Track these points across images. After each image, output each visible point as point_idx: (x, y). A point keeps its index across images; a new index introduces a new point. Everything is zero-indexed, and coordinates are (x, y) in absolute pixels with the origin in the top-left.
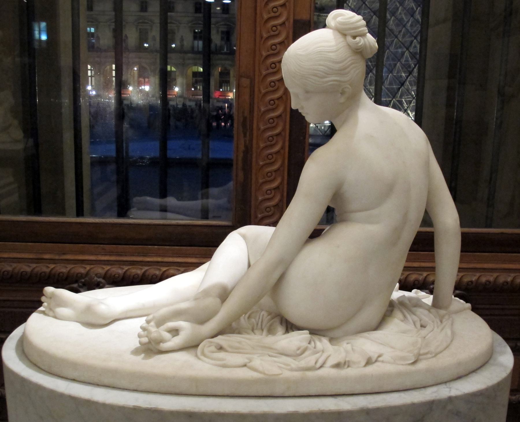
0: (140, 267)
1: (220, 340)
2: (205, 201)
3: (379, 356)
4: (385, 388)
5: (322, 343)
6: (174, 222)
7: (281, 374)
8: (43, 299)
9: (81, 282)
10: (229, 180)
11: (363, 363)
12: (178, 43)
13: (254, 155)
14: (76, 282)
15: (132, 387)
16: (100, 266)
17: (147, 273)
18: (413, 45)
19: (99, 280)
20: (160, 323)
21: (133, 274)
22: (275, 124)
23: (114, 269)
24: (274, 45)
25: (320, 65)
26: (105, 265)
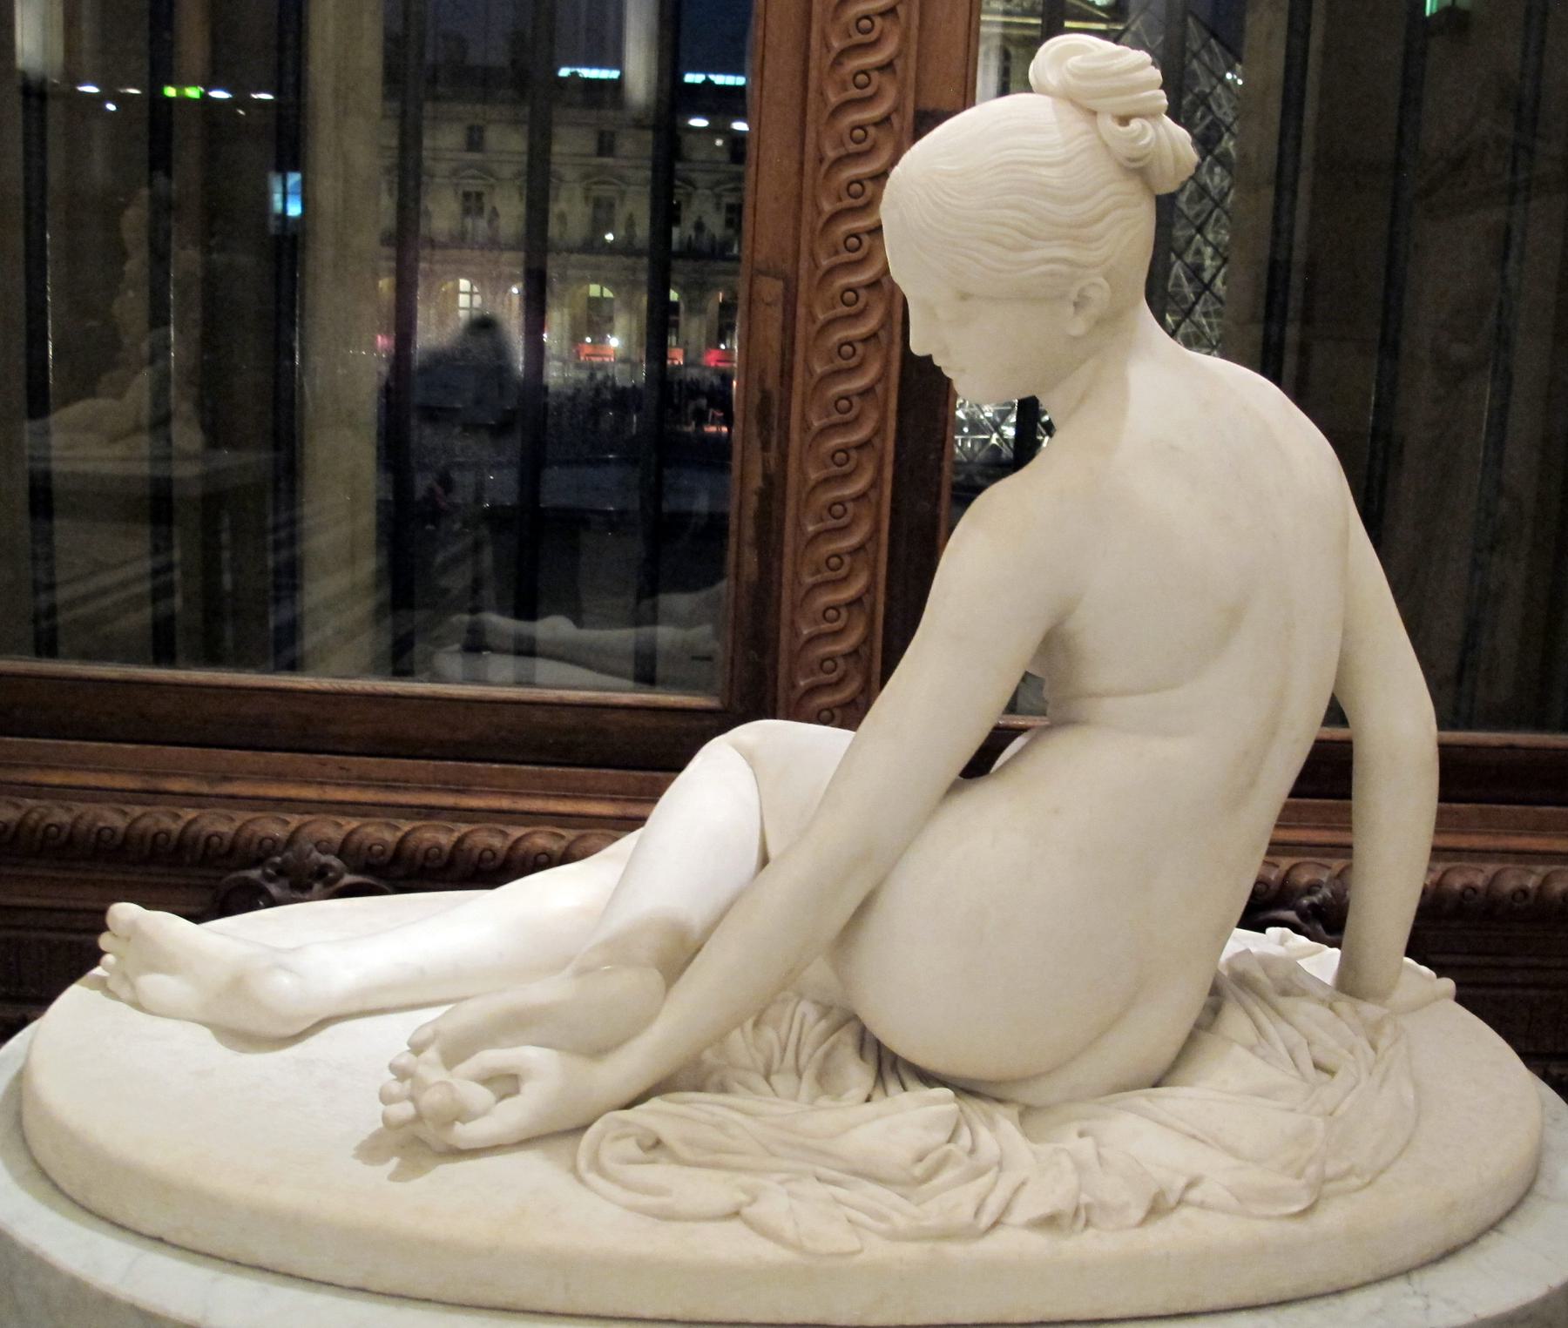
1: (656, 1115)
2: (646, 630)
3: (1190, 1185)
4: (1209, 1302)
5: (997, 1132)
6: (551, 695)
7: (860, 1251)
8: (104, 941)
9: (273, 865)
10: (720, 576)
11: (1137, 1214)
12: (622, 233)
13: (791, 504)
14: (258, 862)
15: (351, 1276)
16: (332, 818)
17: (467, 844)
18: (1193, 247)
19: (324, 859)
20: (455, 1053)
21: (425, 845)
22: (852, 463)
24: (867, 17)
25: (1009, 207)
26: (345, 814)
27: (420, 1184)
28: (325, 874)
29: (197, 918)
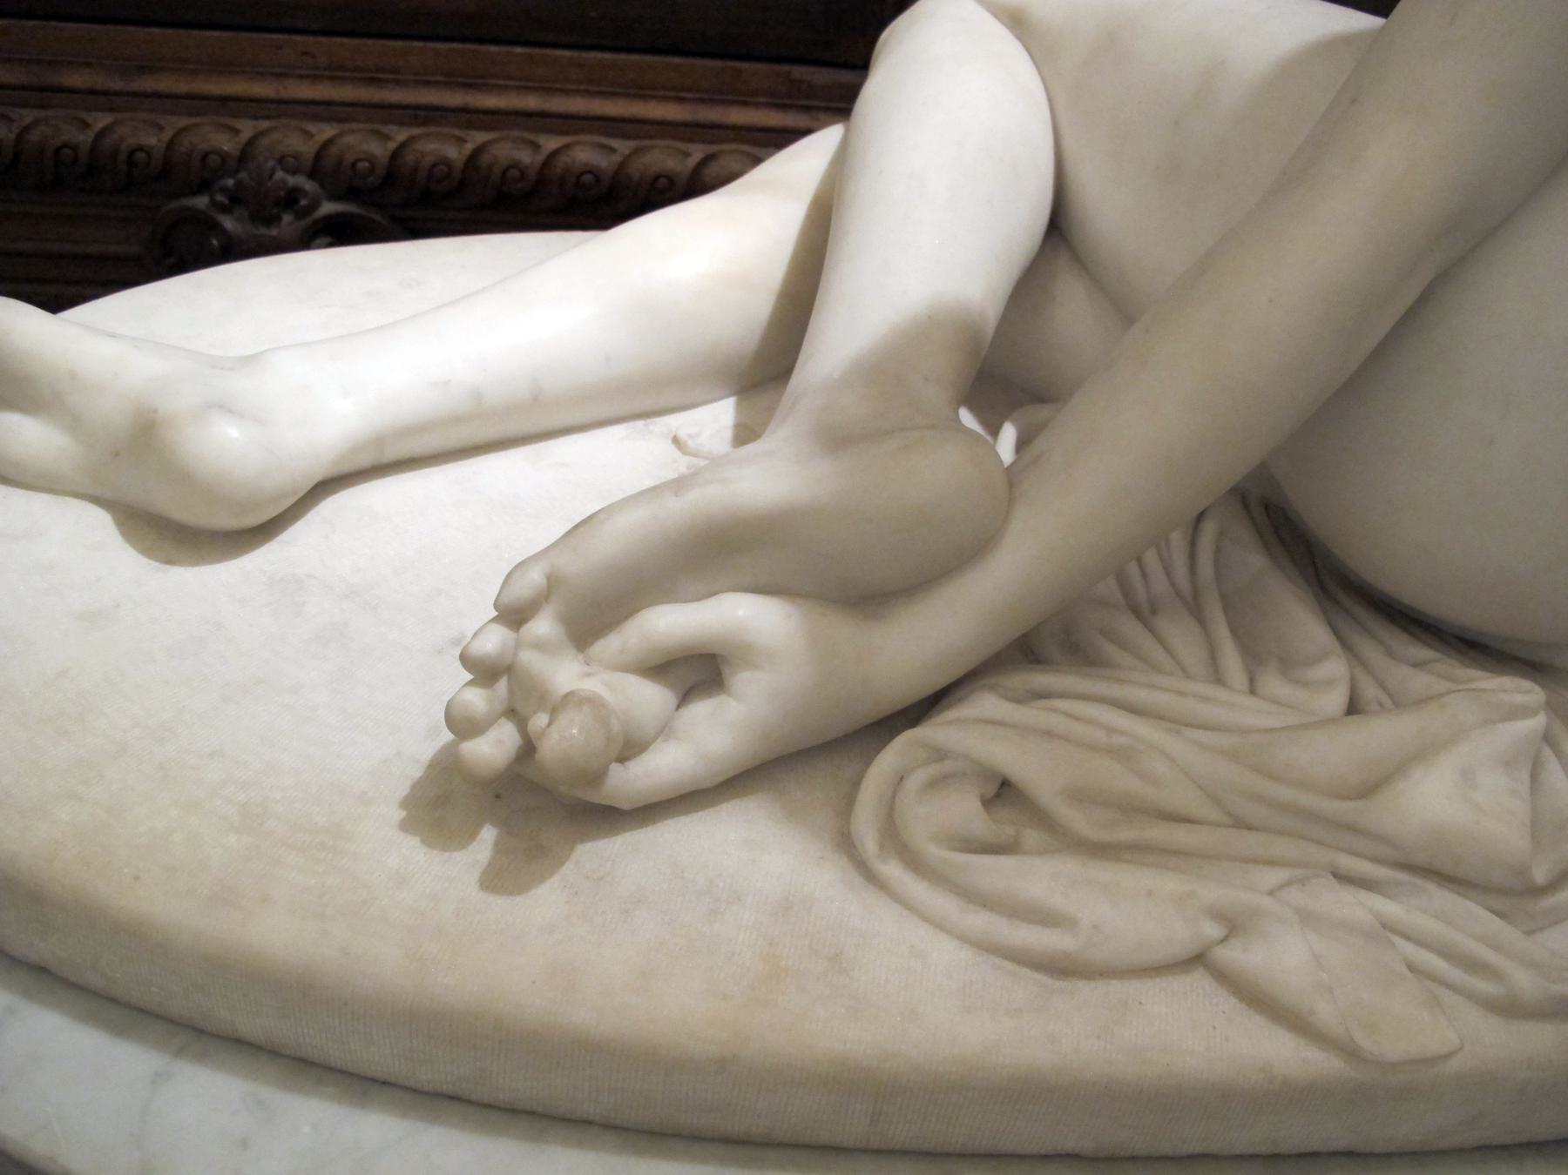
0: (457, 132)
1: (981, 730)
9: (224, 190)
14: (204, 186)
17: (410, 158)
19: (292, 181)
21: (429, 160)
23: (350, 139)
26: (317, 118)
27: (547, 903)
28: (296, 201)
29: (55, 304)
